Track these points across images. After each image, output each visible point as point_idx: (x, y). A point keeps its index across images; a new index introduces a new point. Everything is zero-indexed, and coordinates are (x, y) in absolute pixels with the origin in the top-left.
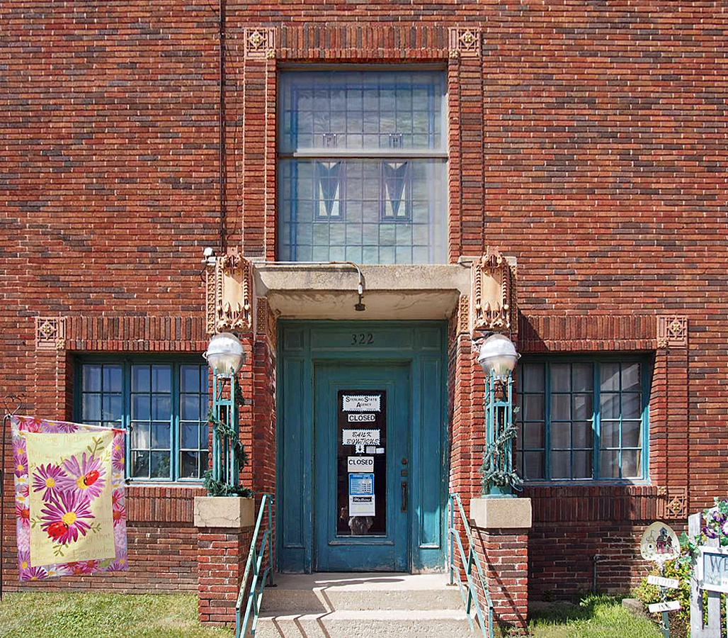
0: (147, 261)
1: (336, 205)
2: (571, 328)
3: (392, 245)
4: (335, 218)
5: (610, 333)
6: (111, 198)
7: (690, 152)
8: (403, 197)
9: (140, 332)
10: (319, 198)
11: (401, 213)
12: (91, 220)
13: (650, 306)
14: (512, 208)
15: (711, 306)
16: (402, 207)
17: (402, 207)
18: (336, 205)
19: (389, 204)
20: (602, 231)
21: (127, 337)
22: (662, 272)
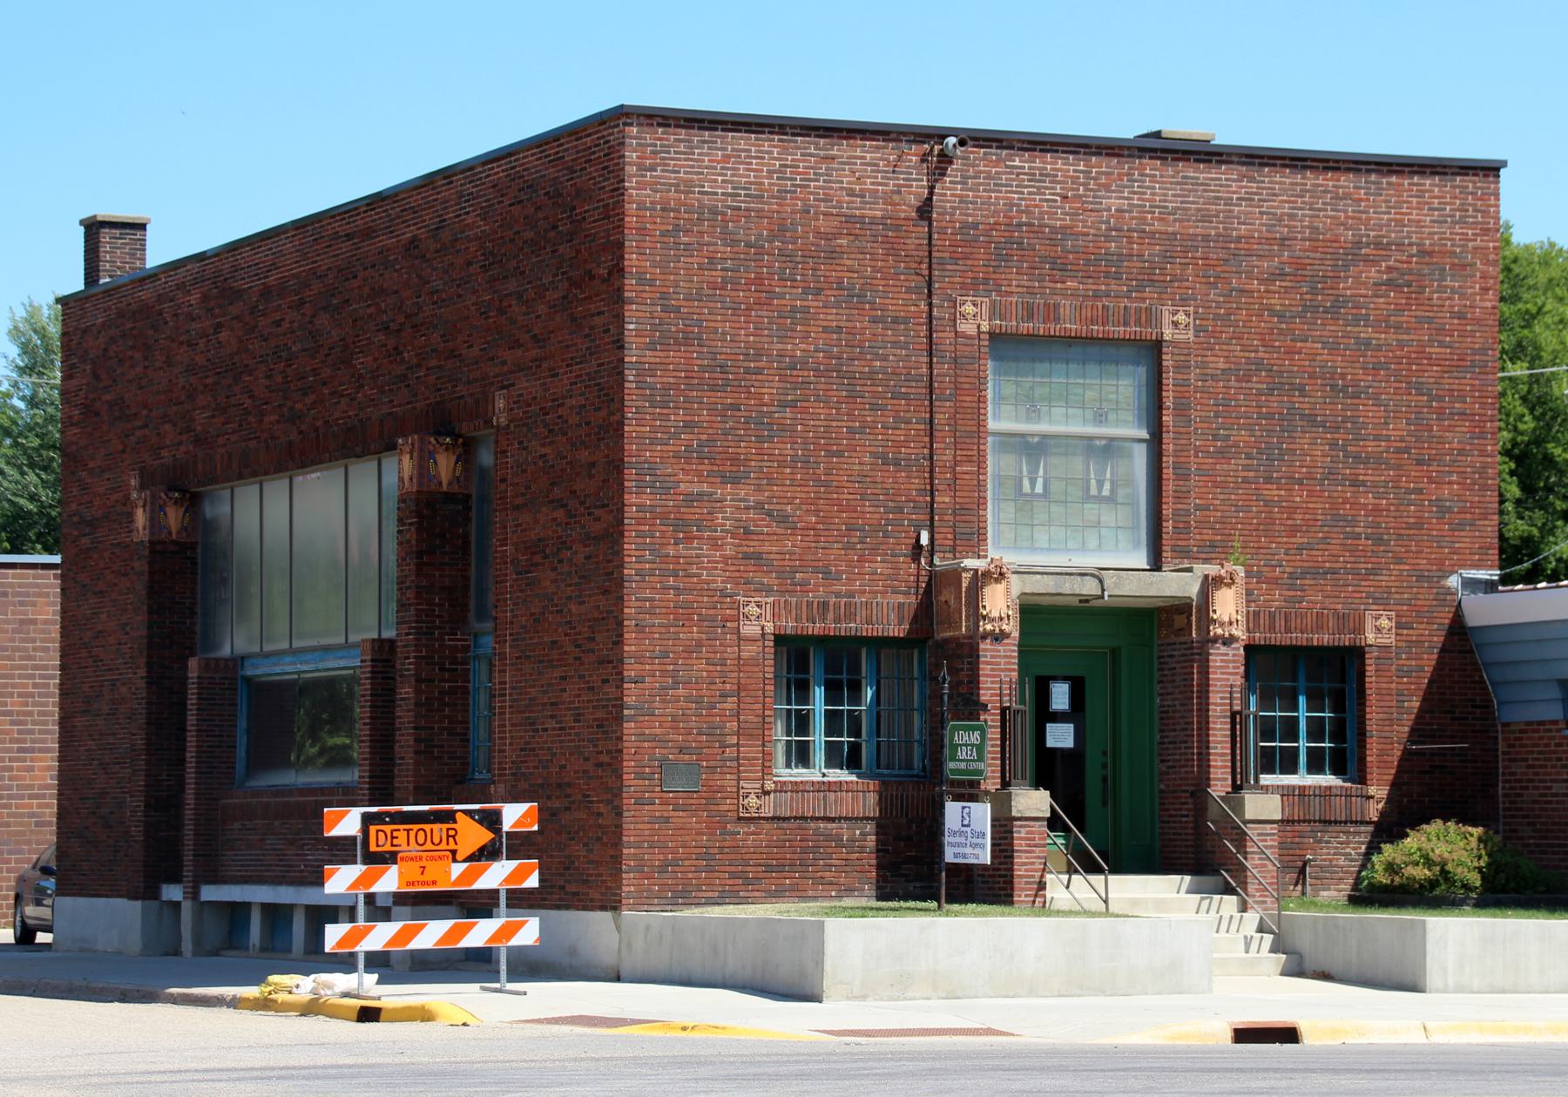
0: (856, 540)
1: (1040, 482)
2: (1280, 623)
3: (1098, 525)
4: (1039, 495)
5: (1319, 628)
6: (818, 471)
7: (1399, 444)
8: (1108, 476)
9: (851, 616)
10: (912, 736)
11: (1106, 491)
12: (798, 495)
13: (1357, 601)
14: (1222, 497)
15: (1419, 603)
16: (1107, 486)
17: (1107, 486)
18: (1040, 482)
19: (1093, 482)
20: (1311, 523)
21: (837, 620)
22: (1370, 566)
